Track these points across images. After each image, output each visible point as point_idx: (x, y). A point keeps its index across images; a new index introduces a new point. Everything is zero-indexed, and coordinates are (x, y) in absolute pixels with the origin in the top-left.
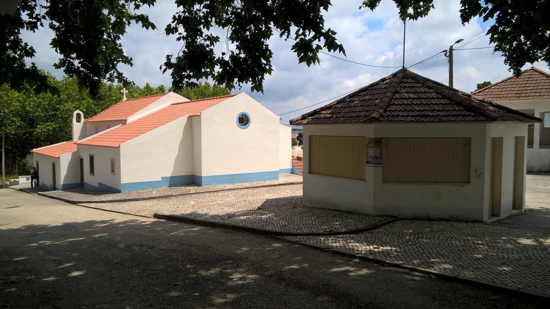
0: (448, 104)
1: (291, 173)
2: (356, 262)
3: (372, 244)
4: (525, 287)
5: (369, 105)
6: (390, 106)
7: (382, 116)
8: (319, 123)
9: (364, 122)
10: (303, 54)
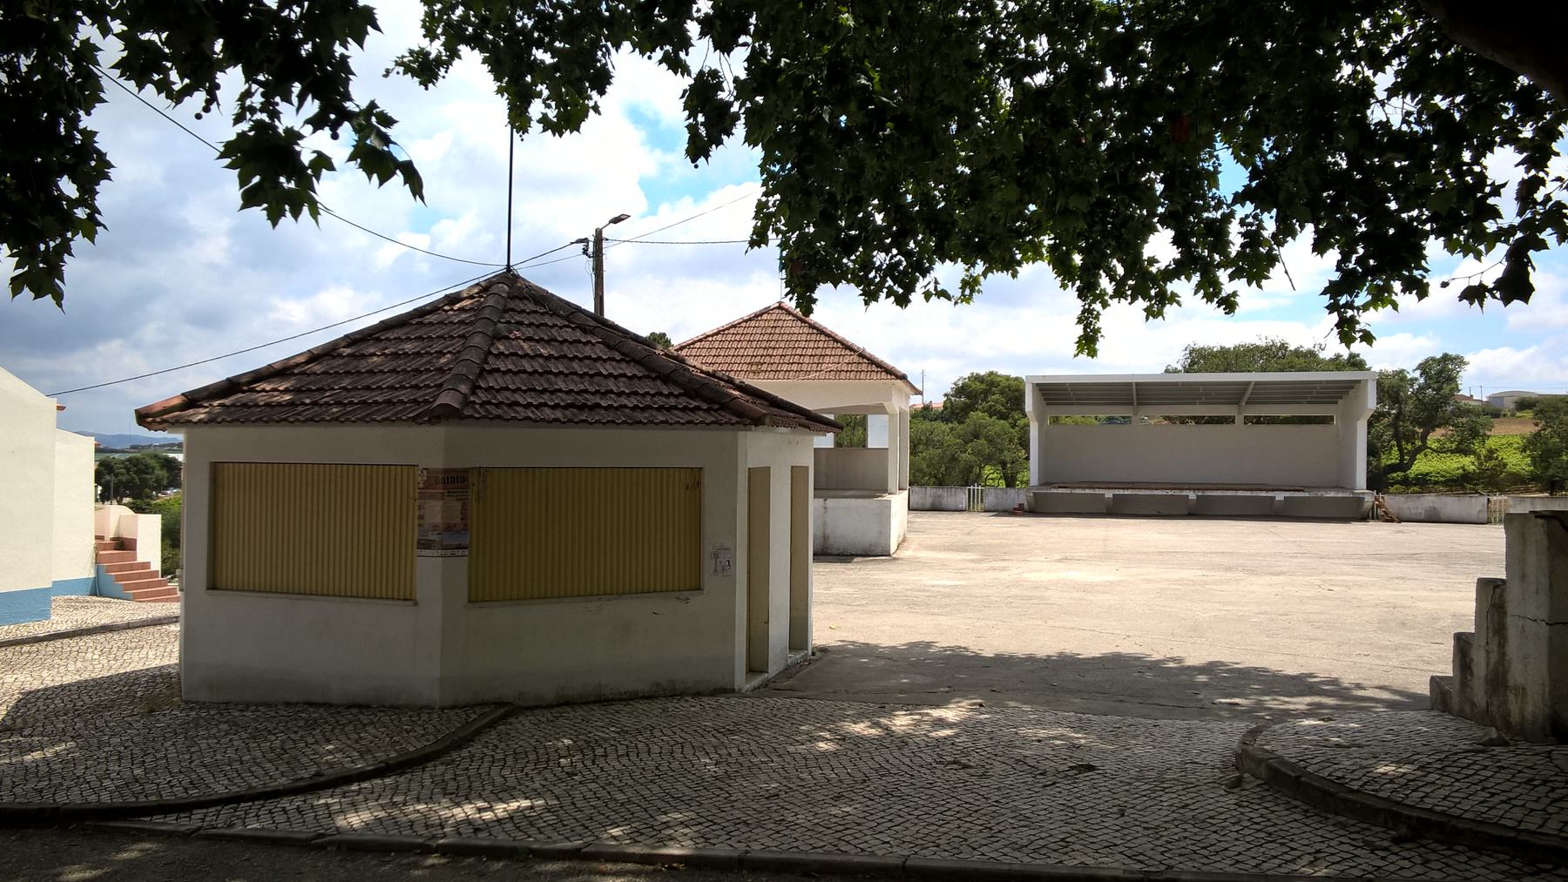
0: (640, 378)
1: (91, 595)
2: (433, 866)
3: (468, 799)
4: (915, 849)
5: (417, 371)
6: (485, 373)
7: (467, 403)
8: (253, 419)
9: (414, 419)
10: (256, 179)
